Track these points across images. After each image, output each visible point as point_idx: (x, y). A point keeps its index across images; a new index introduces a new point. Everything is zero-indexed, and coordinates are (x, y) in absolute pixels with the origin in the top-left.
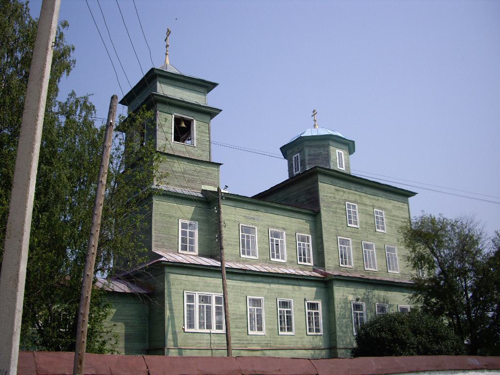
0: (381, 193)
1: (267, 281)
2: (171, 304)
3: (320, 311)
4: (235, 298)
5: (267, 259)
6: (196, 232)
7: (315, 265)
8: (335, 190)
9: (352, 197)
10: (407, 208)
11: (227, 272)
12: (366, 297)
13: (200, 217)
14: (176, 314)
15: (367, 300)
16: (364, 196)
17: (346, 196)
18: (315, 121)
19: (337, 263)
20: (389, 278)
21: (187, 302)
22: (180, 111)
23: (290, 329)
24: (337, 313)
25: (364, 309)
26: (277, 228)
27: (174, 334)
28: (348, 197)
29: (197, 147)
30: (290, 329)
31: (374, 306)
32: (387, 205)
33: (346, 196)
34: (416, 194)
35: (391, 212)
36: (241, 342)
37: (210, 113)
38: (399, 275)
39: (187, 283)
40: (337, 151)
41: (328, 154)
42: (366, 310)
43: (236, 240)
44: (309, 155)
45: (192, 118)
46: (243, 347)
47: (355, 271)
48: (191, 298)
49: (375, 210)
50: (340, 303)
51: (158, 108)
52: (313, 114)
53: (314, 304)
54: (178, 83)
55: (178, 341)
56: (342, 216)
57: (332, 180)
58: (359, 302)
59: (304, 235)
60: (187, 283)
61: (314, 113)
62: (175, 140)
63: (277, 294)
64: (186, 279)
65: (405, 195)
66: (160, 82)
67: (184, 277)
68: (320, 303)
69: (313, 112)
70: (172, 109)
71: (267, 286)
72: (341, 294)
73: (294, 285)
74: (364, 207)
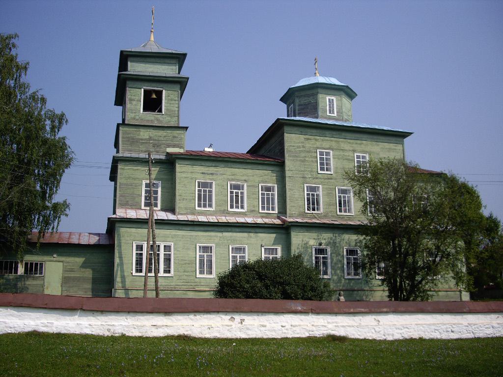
0: (365, 136)
1: (220, 230)
2: (120, 253)
4: (184, 246)
5: (224, 210)
6: (159, 190)
7: (279, 213)
8: (305, 139)
9: (326, 144)
10: (402, 148)
12: (332, 241)
13: (166, 177)
14: (125, 260)
16: (342, 142)
17: (318, 144)
19: (302, 210)
21: (136, 251)
22: (149, 84)
25: (329, 253)
26: (238, 180)
27: (123, 277)
28: (321, 145)
29: (166, 114)
31: (342, 250)
33: (318, 144)
34: (412, 133)
35: (378, 154)
36: (189, 284)
39: (137, 235)
40: (328, 98)
41: (317, 102)
42: (331, 254)
43: (191, 195)
44: (299, 105)
45: (161, 89)
46: (191, 288)
48: (140, 248)
49: (355, 154)
50: (298, 248)
53: (207, 247)
54: (148, 59)
55: (127, 284)
56: (313, 164)
58: (323, 247)
59: (269, 185)
60: (137, 235)
62: (145, 109)
63: (229, 241)
64: (136, 232)
66: (131, 61)
67: (133, 230)
70: (138, 84)
71: (219, 234)
72: (301, 239)
73: (250, 232)
74: (341, 153)
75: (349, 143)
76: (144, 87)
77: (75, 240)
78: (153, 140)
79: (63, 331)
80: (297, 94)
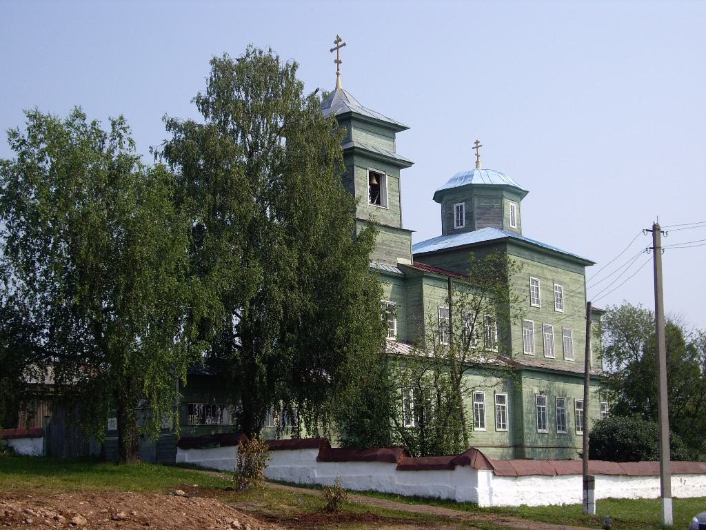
3: (506, 405)
11: (590, 379)
15: (549, 393)
18: (478, 156)
20: (565, 366)
23: (482, 425)
24: (524, 407)
30: (482, 425)
32: (566, 276)
35: (568, 286)
37: (398, 165)
38: (574, 363)
40: (511, 204)
45: (384, 173)
47: (536, 358)
49: (555, 285)
51: (356, 163)
52: (336, 46)
57: (518, 250)
61: (477, 145)
65: (580, 263)
66: (355, 127)
68: (506, 395)
69: (336, 42)
75: (550, 270)
76: (370, 169)
77: (515, 330)
78: (386, 245)
79: (343, 463)
80: (475, 191)
